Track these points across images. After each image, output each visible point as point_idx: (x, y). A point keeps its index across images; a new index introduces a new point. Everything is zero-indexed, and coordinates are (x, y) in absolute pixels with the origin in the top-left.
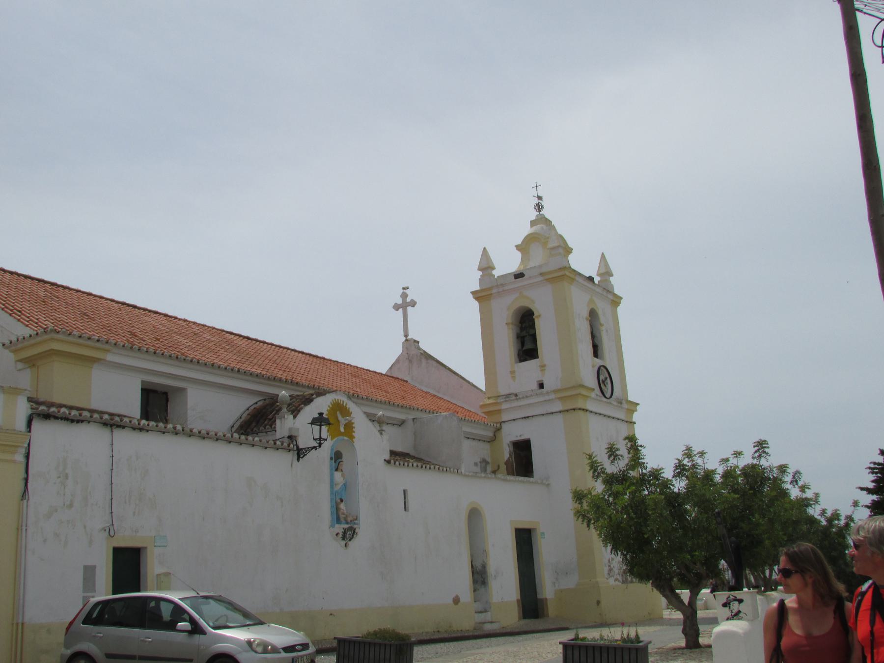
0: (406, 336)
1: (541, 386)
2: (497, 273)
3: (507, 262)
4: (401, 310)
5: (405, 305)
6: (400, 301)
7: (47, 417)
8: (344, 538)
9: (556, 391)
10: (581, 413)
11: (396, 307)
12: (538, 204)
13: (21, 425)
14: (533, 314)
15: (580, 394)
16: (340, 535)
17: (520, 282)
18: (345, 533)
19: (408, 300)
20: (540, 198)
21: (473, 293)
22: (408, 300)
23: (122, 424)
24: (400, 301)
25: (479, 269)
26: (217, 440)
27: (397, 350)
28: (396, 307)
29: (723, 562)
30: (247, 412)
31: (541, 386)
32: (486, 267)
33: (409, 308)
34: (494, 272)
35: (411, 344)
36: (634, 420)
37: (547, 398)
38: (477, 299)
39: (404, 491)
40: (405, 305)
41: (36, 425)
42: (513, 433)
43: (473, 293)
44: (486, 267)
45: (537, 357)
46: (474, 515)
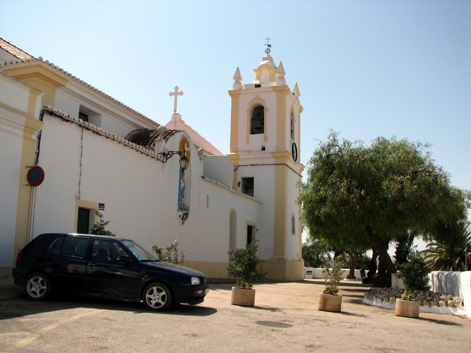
0: (175, 111)
1: (263, 149)
2: (243, 83)
3: (249, 79)
4: (174, 96)
5: (176, 93)
6: (174, 91)
7: (51, 113)
8: (182, 219)
9: (272, 153)
10: (285, 166)
11: (171, 94)
12: (268, 49)
13: (37, 114)
14: (264, 108)
15: (286, 156)
16: (181, 217)
17: (258, 89)
18: (184, 215)
19: (179, 91)
20: (269, 46)
21: (229, 91)
22: (179, 91)
23: (89, 128)
24: (174, 91)
25: (234, 78)
26: (132, 148)
27: (169, 119)
28: (171, 94)
29: (98, 243)
30: (130, 136)
31: (263, 149)
32: (238, 77)
33: (179, 96)
34: (241, 82)
35: (176, 116)
36: (302, 175)
37: (267, 156)
38: (231, 95)
39: (208, 197)
40: (176, 93)
41: (46, 117)
42: (247, 173)
43: (229, 91)
44: (238, 77)
45: (264, 133)
46: (233, 214)
